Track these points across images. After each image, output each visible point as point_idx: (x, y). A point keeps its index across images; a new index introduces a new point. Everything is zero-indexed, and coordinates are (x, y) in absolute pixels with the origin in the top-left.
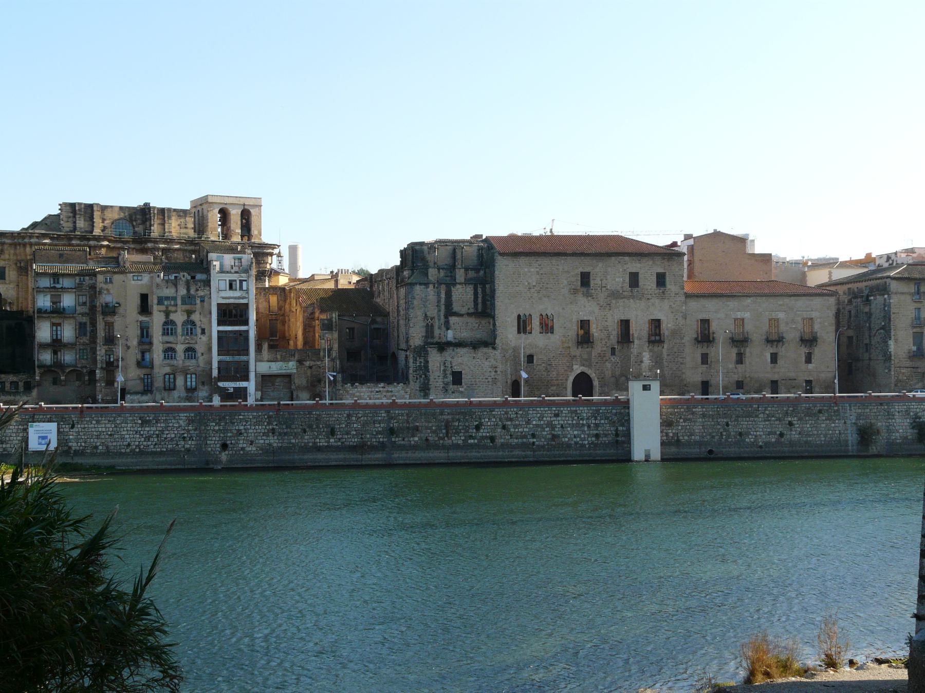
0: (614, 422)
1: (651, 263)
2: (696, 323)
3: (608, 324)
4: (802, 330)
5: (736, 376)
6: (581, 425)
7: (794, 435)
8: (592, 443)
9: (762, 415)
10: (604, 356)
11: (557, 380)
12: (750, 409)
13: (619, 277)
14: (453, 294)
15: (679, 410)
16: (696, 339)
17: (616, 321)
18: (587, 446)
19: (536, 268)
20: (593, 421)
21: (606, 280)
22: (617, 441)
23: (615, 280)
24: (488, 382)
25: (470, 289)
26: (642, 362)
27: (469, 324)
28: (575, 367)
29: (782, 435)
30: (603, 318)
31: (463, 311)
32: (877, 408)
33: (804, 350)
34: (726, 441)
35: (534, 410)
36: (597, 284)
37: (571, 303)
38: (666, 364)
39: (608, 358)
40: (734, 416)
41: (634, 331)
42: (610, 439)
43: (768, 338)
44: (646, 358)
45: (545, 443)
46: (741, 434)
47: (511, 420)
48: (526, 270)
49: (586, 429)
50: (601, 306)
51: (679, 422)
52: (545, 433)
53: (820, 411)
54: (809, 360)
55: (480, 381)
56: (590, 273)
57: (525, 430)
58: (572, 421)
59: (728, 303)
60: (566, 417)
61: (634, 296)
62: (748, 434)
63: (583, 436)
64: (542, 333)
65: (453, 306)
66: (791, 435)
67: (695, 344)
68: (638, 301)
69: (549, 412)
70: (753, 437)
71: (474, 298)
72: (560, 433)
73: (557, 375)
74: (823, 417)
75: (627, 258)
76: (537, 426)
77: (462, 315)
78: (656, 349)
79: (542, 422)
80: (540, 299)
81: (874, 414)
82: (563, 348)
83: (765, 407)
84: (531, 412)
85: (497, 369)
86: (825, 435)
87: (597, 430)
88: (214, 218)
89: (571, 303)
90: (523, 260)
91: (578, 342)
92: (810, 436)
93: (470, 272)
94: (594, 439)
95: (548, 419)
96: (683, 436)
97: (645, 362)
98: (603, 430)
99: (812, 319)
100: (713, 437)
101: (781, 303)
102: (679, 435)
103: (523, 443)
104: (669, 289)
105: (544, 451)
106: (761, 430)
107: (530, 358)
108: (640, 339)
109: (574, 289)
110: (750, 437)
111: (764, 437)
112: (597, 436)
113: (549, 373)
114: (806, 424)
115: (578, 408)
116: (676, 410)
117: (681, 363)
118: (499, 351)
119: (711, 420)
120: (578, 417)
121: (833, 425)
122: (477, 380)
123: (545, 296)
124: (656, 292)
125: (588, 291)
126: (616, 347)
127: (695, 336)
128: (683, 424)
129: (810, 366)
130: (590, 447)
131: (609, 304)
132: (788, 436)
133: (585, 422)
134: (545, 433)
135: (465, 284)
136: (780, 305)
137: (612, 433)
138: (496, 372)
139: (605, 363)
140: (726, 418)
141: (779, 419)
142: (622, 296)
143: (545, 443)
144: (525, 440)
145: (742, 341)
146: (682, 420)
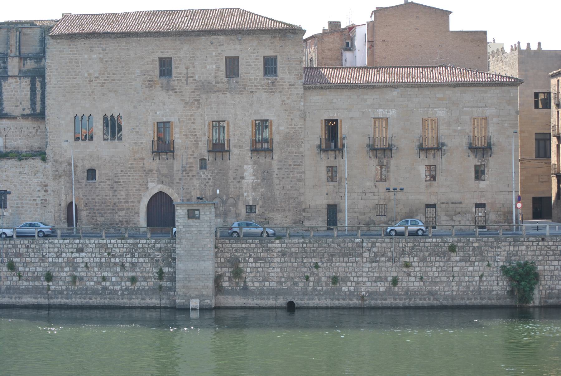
0: (157, 261)
1: (255, 43)
2: (320, 124)
3: (195, 127)
4: (471, 134)
5: (376, 198)
6: (112, 265)
7: (414, 284)
8: (127, 289)
9: (366, 254)
10: (191, 170)
11: (127, 202)
12: (350, 245)
13: (211, 64)
14: (3, 90)
15: (248, 246)
16: (320, 147)
17: (207, 123)
18: (119, 293)
19: (100, 53)
20: (129, 260)
21: (194, 67)
22: (161, 287)
23: (206, 67)
24: (37, 204)
25: (26, 84)
26: (242, 178)
27: (25, 129)
28: (151, 185)
29: (395, 282)
30: (190, 119)
31: (17, 112)
32: (538, 245)
33: (473, 161)
34: (314, 289)
35: (50, 243)
36: (180, 74)
37: (146, 99)
38: (276, 180)
39: (194, 173)
40: (326, 255)
41: (232, 136)
42: (151, 283)
43: (422, 144)
44: (249, 171)
45: (64, 288)
46: (335, 280)
47: (20, 255)
48: (86, 56)
49: (118, 269)
50: (187, 103)
51: (248, 262)
52: (65, 274)
53: (452, 249)
54: (479, 173)
55: (27, 204)
56: (171, 58)
57: (38, 269)
58: (101, 258)
59: (365, 97)
60: (92, 253)
61: (232, 88)
62: (346, 280)
63: (114, 279)
64: (107, 139)
65: (3, 106)
66: (408, 282)
67: (318, 153)
68: (237, 96)
69: (71, 246)
70: (354, 284)
71: (31, 95)
72: (84, 274)
73: (127, 195)
74: (455, 257)
75: (222, 38)
76: (54, 264)
77: (15, 118)
78: (262, 160)
79: (61, 260)
80: (104, 94)
81: (533, 253)
82: (135, 159)
83: (373, 243)
84: (46, 246)
85: (47, 188)
86: (459, 284)
87: (133, 271)
88: (244, 12)
89: (146, 99)
90: (81, 44)
91: (153, 152)
92: (436, 283)
93: (28, 61)
94: (129, 283)
95: (69, 255)
96: (253, 282)
97: (246, 178)
98: (142, 272)
99: (485, 118)
100: (296, 284)
101: (440, 96)
102: (247, 280)
103: (36, 287)
104: (282, 79)
105: (62, 298)
106: (365, 274)
107: (91, 173)
108: (240, 147)
109: (149, 81)
110: (349, 284)
111: (369, 284)
112: (133, 280)
113: (116, 193)
114: (432, 266)
115: (108, 242)
116: (244, 246)
117: (299, 180)
118: (50, 164)
119: (293, 260)
120: (109, 254)
121: (471, 269)
122: (24, 202)
123: (110, 91)
124: (263, 82)
125: (168, 83)
126: (206, 158)
127: (318, 142)
128: (254, 265)
129: (483, 184)
130: (122, 294)
131: (198, 100)
132: (405, 284)
133: (117, 260)
134: (65, 274)
135: (20, 77)
136: (440, 99)
137: (154, 277)
138: (46, 191)
139: (191, 179)
140: (314, 257)
141: (392, 260)
142: (216, 90)
143: (64, 288)
144: (37, 283)
145: (384, 150)
146: (251, 260)
